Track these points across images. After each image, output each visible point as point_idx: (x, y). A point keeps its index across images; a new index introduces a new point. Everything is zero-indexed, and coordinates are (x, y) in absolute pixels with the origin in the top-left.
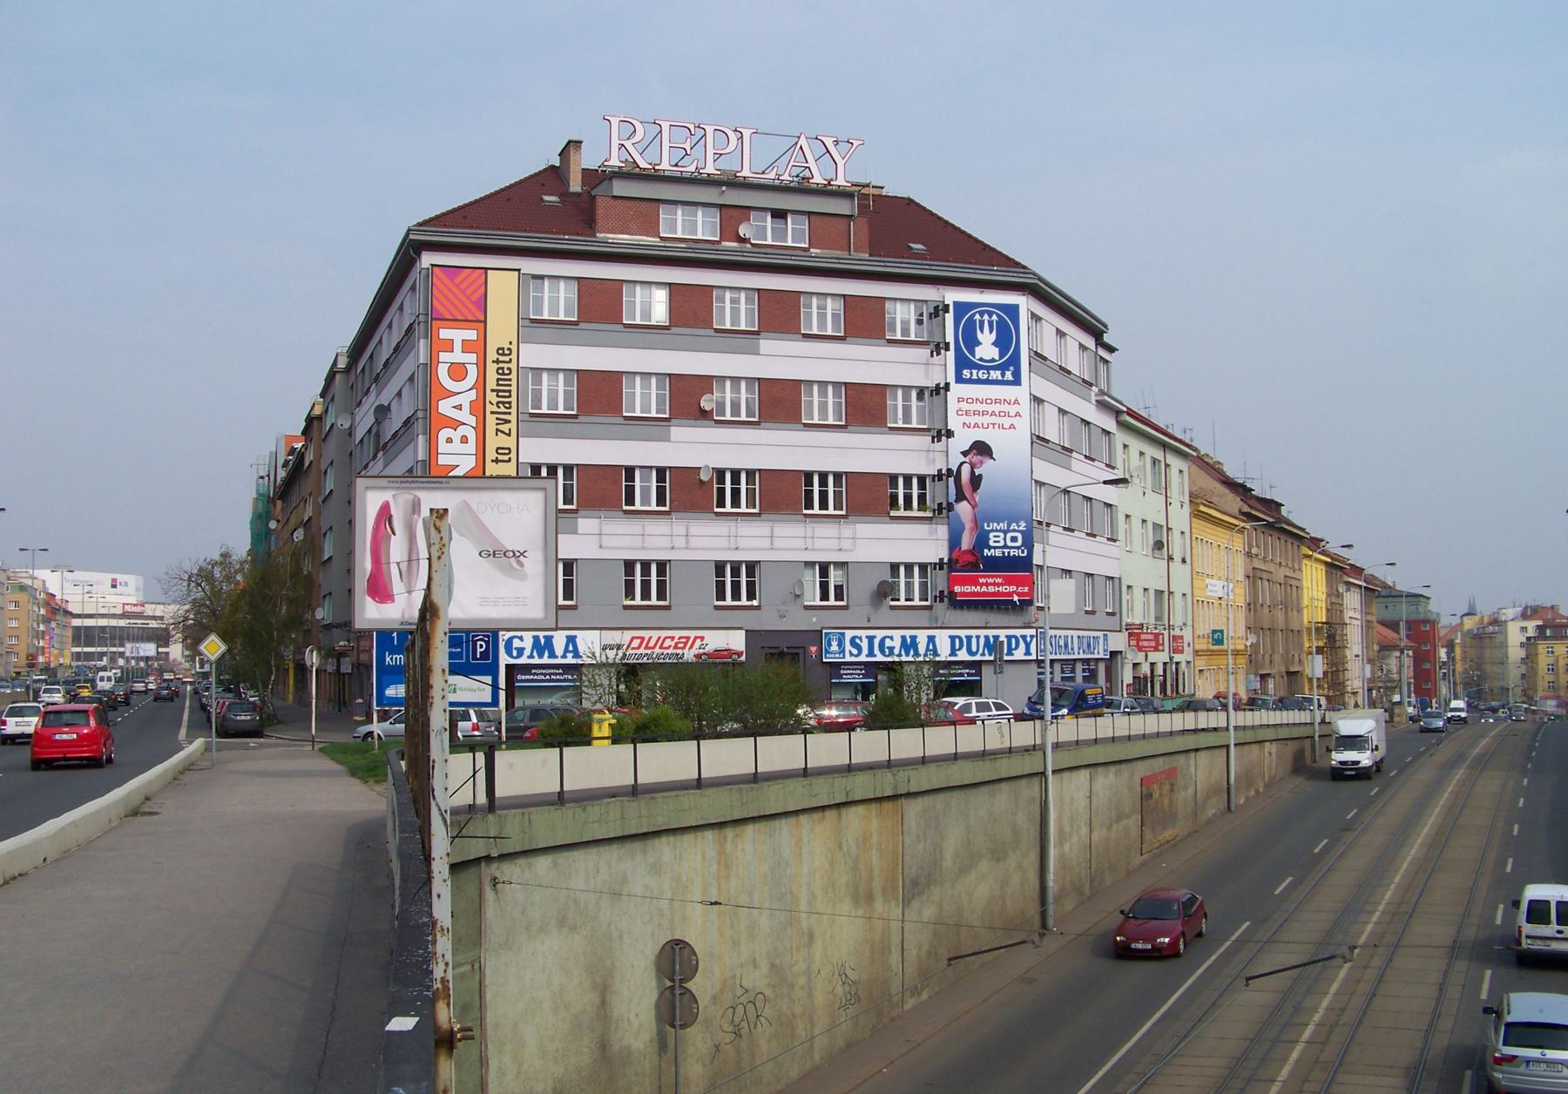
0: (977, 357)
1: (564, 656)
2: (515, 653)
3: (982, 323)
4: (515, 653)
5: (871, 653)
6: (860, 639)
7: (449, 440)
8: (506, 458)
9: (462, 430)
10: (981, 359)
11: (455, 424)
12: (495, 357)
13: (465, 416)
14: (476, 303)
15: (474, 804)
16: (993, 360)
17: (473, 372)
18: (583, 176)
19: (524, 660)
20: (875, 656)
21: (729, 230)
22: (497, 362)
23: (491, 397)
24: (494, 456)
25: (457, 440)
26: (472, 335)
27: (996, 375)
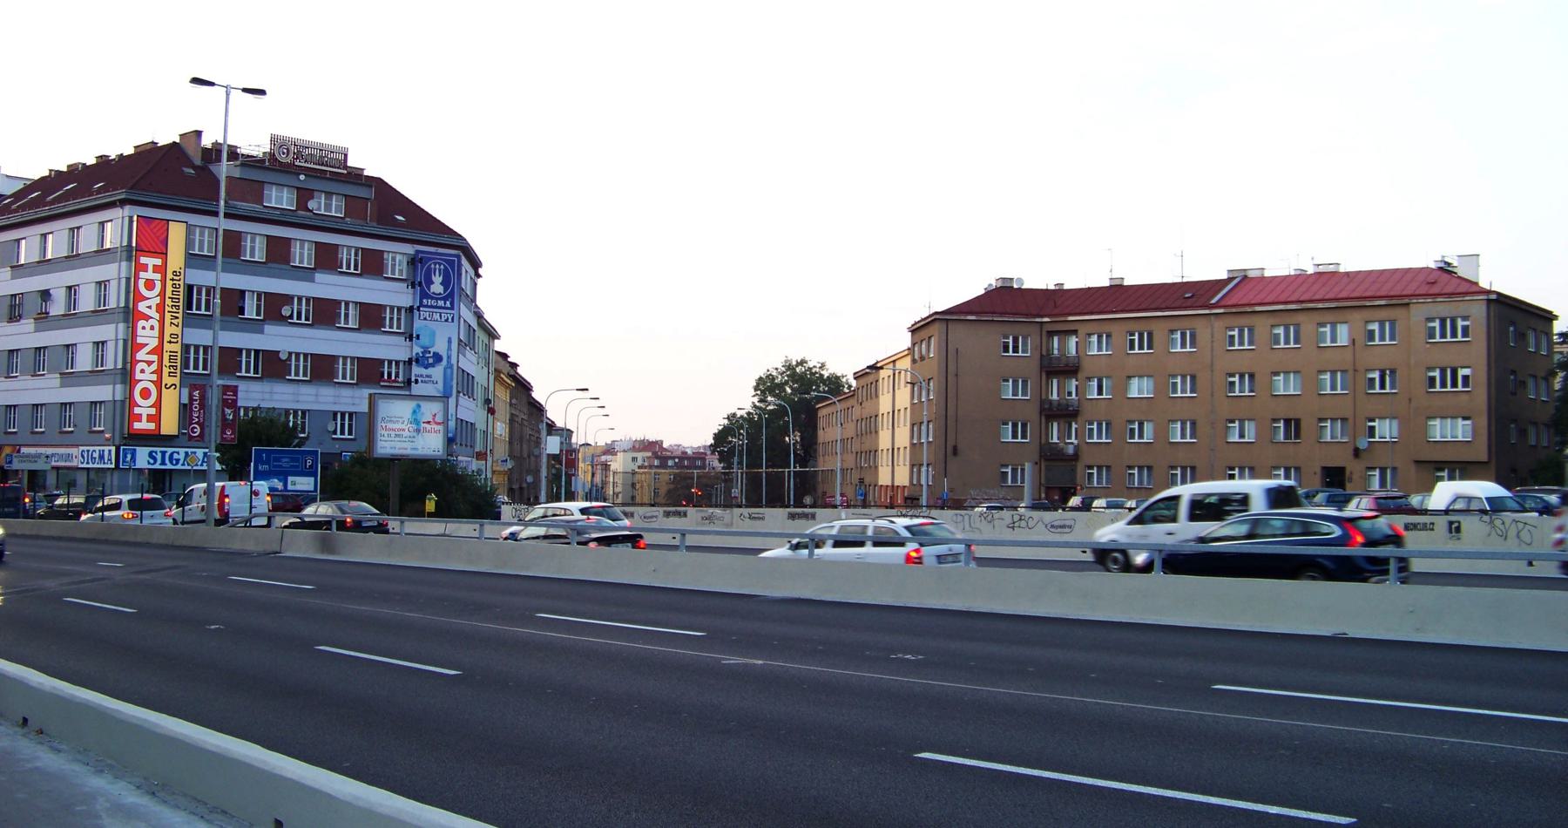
0: (432, 291)
1: (202, 465)
2: (174, 462)
3: (435, 269)
4: (174, 462)
5: (163, 463)
6: (156, 453)
7: (144, 328)
8: (175, 340)
9: (151, 322)
10: (433, 293)
11: (147, 318)
12: (172, 276)
13: (153, 313)
14: (162, 242)
15: (893, 486)
16: (440, 294)
17: (158, 285)
18: (203, 154)
19: (179, 467)
20: (166, 465)
21: (302, 204)
22: (173, 280)
23: (168, 302)
24: (169, 339)
25: (148, 327)
26: (159, 262)
27: (441, 303)
